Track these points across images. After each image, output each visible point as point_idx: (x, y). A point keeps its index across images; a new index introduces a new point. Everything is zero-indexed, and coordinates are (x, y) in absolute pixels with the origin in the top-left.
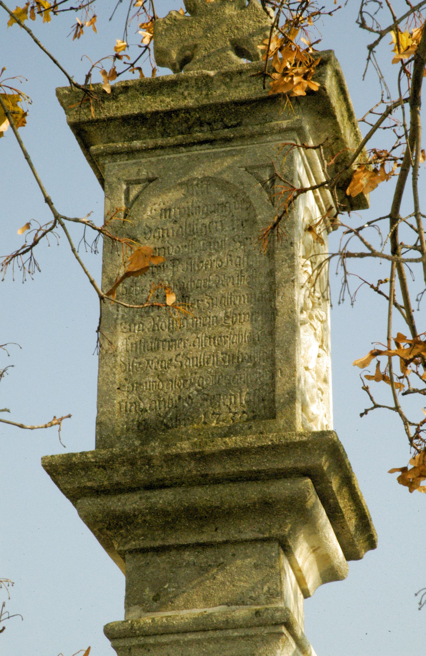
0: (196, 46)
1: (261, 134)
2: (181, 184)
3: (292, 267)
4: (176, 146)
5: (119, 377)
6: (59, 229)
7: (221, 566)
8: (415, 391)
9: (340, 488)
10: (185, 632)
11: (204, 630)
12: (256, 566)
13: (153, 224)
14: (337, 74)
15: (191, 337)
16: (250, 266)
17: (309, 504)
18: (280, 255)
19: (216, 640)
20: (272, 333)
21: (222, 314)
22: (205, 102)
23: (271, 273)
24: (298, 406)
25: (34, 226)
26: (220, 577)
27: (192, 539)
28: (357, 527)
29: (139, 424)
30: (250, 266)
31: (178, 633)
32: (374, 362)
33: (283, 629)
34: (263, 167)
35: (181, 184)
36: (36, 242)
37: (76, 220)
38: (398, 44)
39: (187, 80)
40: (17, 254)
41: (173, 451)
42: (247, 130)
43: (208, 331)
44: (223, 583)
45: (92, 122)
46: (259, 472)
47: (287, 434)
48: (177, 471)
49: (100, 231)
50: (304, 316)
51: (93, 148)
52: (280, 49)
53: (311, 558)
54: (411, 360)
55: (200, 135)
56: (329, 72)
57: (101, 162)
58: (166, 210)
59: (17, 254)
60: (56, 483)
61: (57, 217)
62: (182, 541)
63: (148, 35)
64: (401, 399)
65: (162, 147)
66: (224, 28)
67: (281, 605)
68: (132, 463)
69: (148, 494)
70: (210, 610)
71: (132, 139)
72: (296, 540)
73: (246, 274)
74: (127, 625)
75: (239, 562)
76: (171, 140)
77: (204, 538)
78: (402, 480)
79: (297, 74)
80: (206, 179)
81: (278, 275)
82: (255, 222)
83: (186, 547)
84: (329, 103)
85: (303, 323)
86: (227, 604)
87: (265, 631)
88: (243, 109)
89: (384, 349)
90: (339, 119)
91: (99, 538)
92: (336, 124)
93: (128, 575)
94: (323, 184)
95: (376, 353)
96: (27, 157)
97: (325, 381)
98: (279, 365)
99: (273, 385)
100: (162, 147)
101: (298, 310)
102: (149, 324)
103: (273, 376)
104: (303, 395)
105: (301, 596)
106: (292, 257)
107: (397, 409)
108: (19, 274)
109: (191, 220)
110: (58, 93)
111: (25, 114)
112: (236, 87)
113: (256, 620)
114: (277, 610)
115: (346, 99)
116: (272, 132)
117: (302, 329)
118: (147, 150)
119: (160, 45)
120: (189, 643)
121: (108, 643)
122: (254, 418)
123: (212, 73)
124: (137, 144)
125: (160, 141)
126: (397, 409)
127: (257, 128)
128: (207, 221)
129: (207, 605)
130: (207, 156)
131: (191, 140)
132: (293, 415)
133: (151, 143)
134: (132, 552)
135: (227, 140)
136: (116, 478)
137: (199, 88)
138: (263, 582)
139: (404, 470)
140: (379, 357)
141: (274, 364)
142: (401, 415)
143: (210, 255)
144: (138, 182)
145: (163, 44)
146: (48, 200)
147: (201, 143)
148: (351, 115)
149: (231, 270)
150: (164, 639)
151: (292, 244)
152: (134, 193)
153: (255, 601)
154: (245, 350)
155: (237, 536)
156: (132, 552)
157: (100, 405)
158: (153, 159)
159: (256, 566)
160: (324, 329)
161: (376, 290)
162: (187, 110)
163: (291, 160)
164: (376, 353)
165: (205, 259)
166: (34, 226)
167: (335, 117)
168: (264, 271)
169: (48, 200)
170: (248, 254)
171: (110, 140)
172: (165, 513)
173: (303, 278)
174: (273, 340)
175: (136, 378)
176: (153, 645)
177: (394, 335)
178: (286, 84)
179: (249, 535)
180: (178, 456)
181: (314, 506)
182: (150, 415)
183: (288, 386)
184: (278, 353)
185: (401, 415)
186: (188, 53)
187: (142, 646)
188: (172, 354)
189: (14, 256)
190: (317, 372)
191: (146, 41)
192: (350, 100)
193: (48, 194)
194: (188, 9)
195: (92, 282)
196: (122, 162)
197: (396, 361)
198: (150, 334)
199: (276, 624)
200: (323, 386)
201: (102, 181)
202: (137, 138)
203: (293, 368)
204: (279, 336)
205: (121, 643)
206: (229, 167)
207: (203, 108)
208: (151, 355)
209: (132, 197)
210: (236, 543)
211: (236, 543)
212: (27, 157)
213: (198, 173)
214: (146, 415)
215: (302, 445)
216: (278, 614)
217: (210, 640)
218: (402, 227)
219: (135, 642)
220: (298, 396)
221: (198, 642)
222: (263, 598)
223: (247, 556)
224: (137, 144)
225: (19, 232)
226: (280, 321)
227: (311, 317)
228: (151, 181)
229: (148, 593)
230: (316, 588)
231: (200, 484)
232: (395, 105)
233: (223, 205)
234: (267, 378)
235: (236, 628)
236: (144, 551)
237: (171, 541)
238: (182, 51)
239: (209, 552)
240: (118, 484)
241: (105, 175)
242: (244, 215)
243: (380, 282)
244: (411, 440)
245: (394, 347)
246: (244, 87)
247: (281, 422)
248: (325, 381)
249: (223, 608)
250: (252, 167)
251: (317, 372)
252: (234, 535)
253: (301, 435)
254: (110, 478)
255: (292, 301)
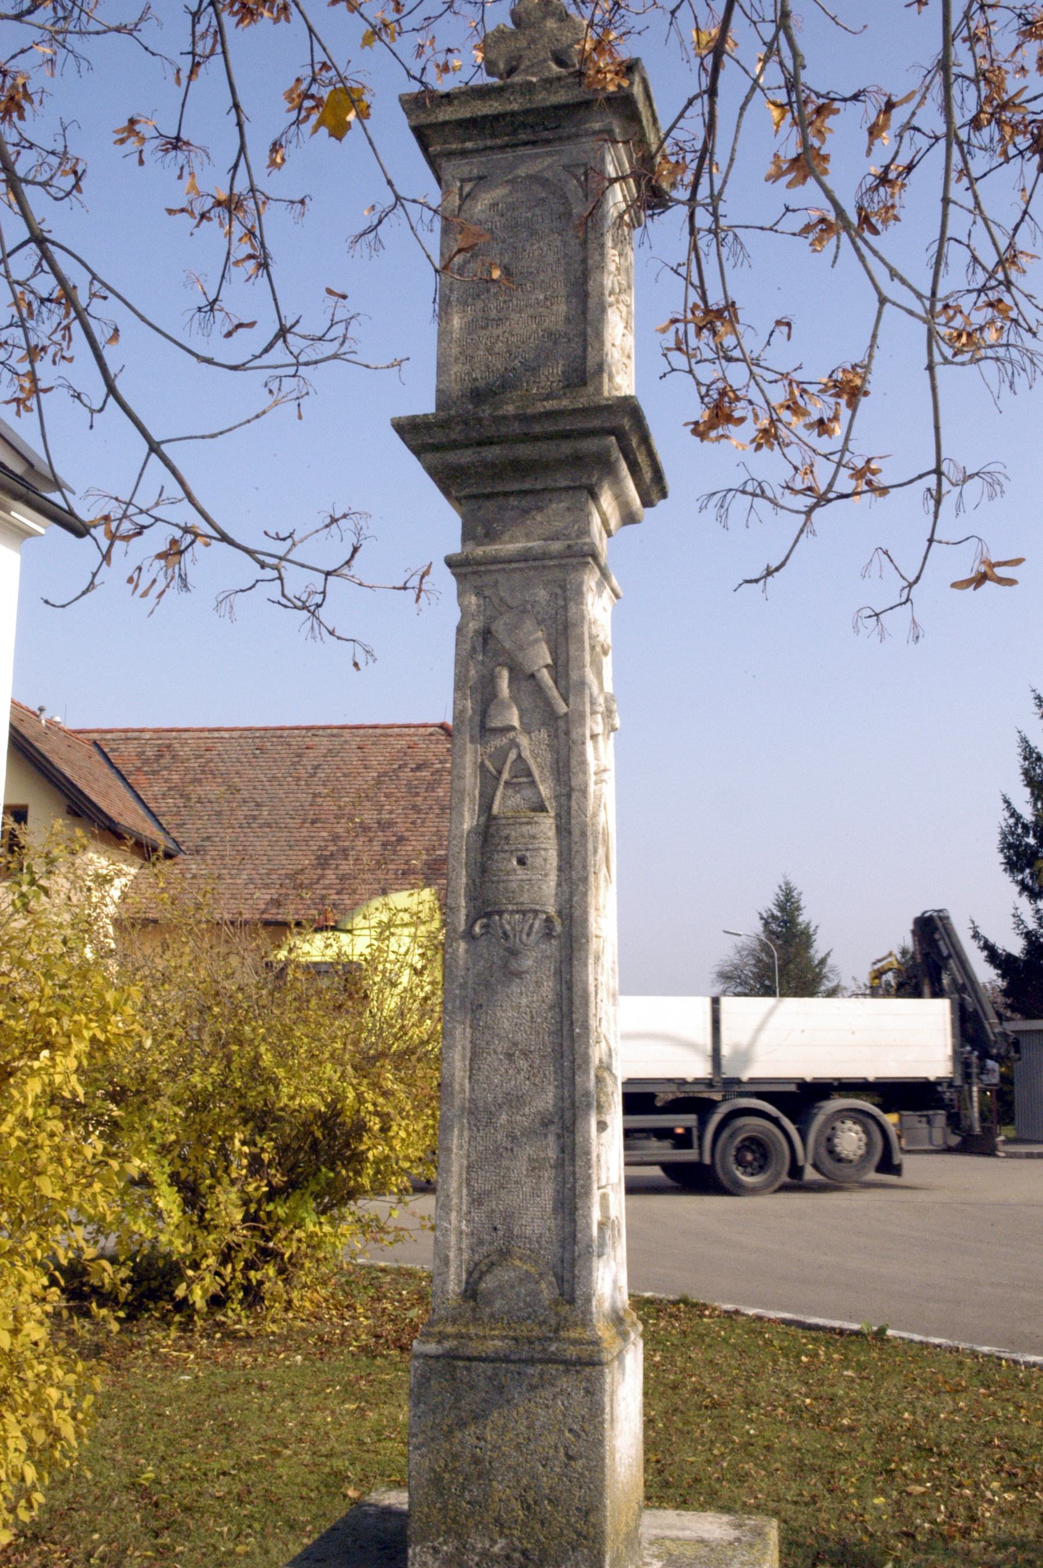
0: (521, 57)
1: (578, 136)
2: (507, 182)
3: (603, 255)
4: (503, 148)
5: (455, 351)
6: (399, 210)
7: (540, 509)
8: (705, 360)
9: (639, 446)
10: (510, 561)
11: (526, 560)
12: (568, 509)
13: (482, 217)
14: (644, 82)
15: (515, 316)
16: (566, 255)
17: (613, 458)
18: (592, 245)
19: (535, 568)
20: (584, 313)
21: (542, 297)
22: (528, 106)
23: (584, 261)
24: (605, 377)
25: (379, 208)
26: (539, 518)
27: (516, 486)
28: (652, 480)
29: (472, 391)
30: (566, 255)
31: (505, 562)
32: (673, 328)
33: (590, 560)
34: (578, 166)
35: (507, 182)
36: (380, 222)
37: (414, 201)
38: (698, 42)
39: (512, 85)
40: (364, 234)
41: (501, 412)
42: (564, 132)
43: (531, 311)
44: (541, 523)
45: (430, 126)
46: (571, 431)
47: (596, 399)
48: (503, 430)
49: (435, 211)
50: (612, 299)
51: (431, 149)
52: (595, 49)
53: (614, 504)
54: (704, 327)
55: (523, 137)
56: (637, 79)
57: (438, 161)
58: (494, 205)
59: (364, 234)
60: (403, 439)
61: (398, 198)
62: (507, 489)
63: (481, 55)
64: (694, 366)
65: (491, 148)
66: (546, 39)
67: (587, 540)
68: (466, 423)
69: (479, 449)
70: (530, 545)
71: (464, 142)
72: (601, 488)
73: (563, 262)
74: (463, 556)
75: (554, 506)
76: (499, 142)
77: (527, 486)
78: (695, 432)
79: (610, 71)
80: (529, 177)
81: (590, 262)
82: (570, 215)
83: (513, 493)
84: (637, 108)
85: (611, 305)
86: (545, 540)
87: (574, 561)
88: (561, 113)
89: (681, 317)
90: (645, 123)
91: (439, 486)
92: (642, 128)
93: (463, 516)
94: (628, 176)
95: (674, 321)
96: (371, 143)
97: (629, 357)
98: (589, 340)
99: (585, 358)
100: (491, 148)
101: (607, 292)
102: (480, 305)
103: (585, 350)
104: (610, 366)
105: (604, 535)
106: (602, 246)
107: (691, 372)
108: (366, 252)
109: (516, 213)
110: (400, 100)
111: (369, 107)
112: (556, 92)
113: (567, 553)
114: (585, 544)
115: (651, 105)
116: (587, 133)
117: (610, 311)
118: (477, 151)
119: (489, 56)
120: (514, 570)
121: (448, 571)
122: (568, 386)
123: (534, 80)
124: (469, 145)
125: (489, 143)
126: (691, 372)
127: (573, 130)
128: (529, 215)
129: (528, 541)
130: (530, 156)
131: (515, 141)
132: (601, 383)
133: (481, 144)
134: (468, 497)
135: (547, 142)
136: (453, 436)
137: (522, 94)
138: (575, 522)
139: (696, 423)
140: (678, 325)
141: (585, 340)
142: (694, 377)
143: (532, 245)
144: (470, 180)
145: (492, 56)
146: (390, 183)
147: (525, 144)
148: (655, 121)
149: (551, 258)
150: (494, 567)
151: (602, 235)
152: (467, 188)
153: (567, 537)
154: (561, 327)
155: (553, 484)
156: (468, 497)
157: (439, 375)
158: (483, 159)
159: (568, 509)
160: (629, 313)
161: (676, 272)
162: (513, 114)
163: (603, 160)
164: (674, 321)
165: (528, 248)
166: (379, 208)
167: (640, 121)
168: (579, 258)
169: (390, 183)
170: (565, 244)
171: (446, 142)
172: (493, 465)
173: (612, 267)
174: (585, 318)
175: (469, 352)
176: (485, 572)
177: (690, 305)
178: (599, 81)
179: (563, 483)
180: (504, 418)
181: (617, 460)
182: (481, 384)
183: (597, 359)
184: (589, 330)
185: (694, 377)
186: (514, 63)
187: (475, 573)
188: (499, 331)
189: (361, 235)
190: (623, 350)
191: (479, 60)
192: (655, 106)
193: (390, 176)
194: (514, 23)
195: (428, 257)
196: (456, 162)
197: (692, 328)
198: (480, 314)
199: (585, 555)
200: (626, 361)
201: (439, 180)
202: (470, 140)
203: (602, 343)
204: (590, 316)
205: (458, 570)
206: (550, 166)
207: (526, 112)
208: (482, 333)
209: (465, 193)
210: (553, 490)
211: (553, 490)
212: (371, 143)
213: (522, 171)
214: (477, 384)
215: (608, 407)
216: (586, 548)
217: (530, 568)
218: (700, 212)
219: (470, 569)
220: (606, 367)
221: (521, 570)
222: (573, 535)
223: (561, 501)
224: (469, 145)
225: (366, 213)
226: (592, 302)
227: (618, 302)
228: (481, 178)
229: (480, 530)
230: (618, 529)
231: (523, 442)
232: (695, 97)
233: (543, 200)
234: (579, 352)
235: (551, 558)
236: (476, 497)
237: (499, 488)
238: (508, 62)
239: (529, 498)
240: (455, 441)
241: (441, 174)
242: (562, 209)
243: (679, 265)
244: (702, 398)
245: (690, 316)
246: (562, 92)
247: (591, 389)
248: (629, 357)
249: (541, 543)
250: (569, 166)
251: (623, 350)
252: (551, 484)
253: (607, 399)
254: (448, 436)
255: (602, 285)
